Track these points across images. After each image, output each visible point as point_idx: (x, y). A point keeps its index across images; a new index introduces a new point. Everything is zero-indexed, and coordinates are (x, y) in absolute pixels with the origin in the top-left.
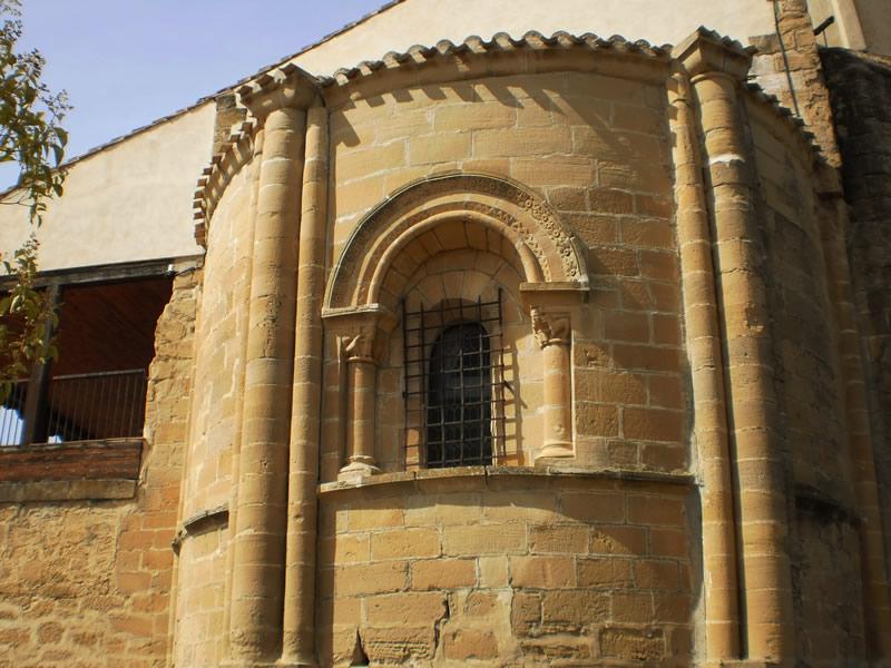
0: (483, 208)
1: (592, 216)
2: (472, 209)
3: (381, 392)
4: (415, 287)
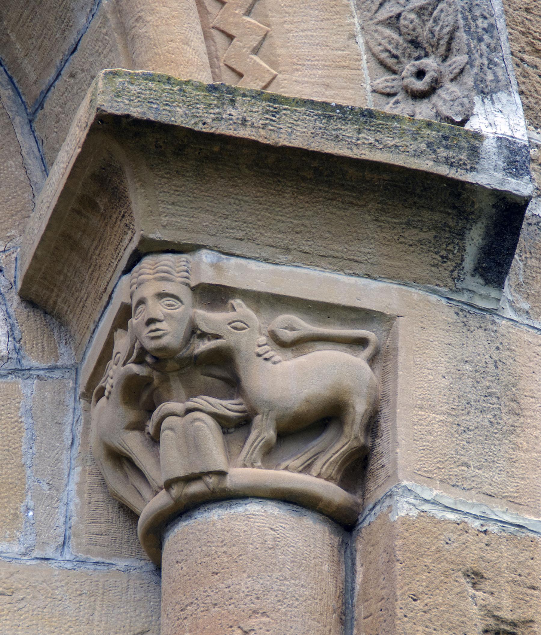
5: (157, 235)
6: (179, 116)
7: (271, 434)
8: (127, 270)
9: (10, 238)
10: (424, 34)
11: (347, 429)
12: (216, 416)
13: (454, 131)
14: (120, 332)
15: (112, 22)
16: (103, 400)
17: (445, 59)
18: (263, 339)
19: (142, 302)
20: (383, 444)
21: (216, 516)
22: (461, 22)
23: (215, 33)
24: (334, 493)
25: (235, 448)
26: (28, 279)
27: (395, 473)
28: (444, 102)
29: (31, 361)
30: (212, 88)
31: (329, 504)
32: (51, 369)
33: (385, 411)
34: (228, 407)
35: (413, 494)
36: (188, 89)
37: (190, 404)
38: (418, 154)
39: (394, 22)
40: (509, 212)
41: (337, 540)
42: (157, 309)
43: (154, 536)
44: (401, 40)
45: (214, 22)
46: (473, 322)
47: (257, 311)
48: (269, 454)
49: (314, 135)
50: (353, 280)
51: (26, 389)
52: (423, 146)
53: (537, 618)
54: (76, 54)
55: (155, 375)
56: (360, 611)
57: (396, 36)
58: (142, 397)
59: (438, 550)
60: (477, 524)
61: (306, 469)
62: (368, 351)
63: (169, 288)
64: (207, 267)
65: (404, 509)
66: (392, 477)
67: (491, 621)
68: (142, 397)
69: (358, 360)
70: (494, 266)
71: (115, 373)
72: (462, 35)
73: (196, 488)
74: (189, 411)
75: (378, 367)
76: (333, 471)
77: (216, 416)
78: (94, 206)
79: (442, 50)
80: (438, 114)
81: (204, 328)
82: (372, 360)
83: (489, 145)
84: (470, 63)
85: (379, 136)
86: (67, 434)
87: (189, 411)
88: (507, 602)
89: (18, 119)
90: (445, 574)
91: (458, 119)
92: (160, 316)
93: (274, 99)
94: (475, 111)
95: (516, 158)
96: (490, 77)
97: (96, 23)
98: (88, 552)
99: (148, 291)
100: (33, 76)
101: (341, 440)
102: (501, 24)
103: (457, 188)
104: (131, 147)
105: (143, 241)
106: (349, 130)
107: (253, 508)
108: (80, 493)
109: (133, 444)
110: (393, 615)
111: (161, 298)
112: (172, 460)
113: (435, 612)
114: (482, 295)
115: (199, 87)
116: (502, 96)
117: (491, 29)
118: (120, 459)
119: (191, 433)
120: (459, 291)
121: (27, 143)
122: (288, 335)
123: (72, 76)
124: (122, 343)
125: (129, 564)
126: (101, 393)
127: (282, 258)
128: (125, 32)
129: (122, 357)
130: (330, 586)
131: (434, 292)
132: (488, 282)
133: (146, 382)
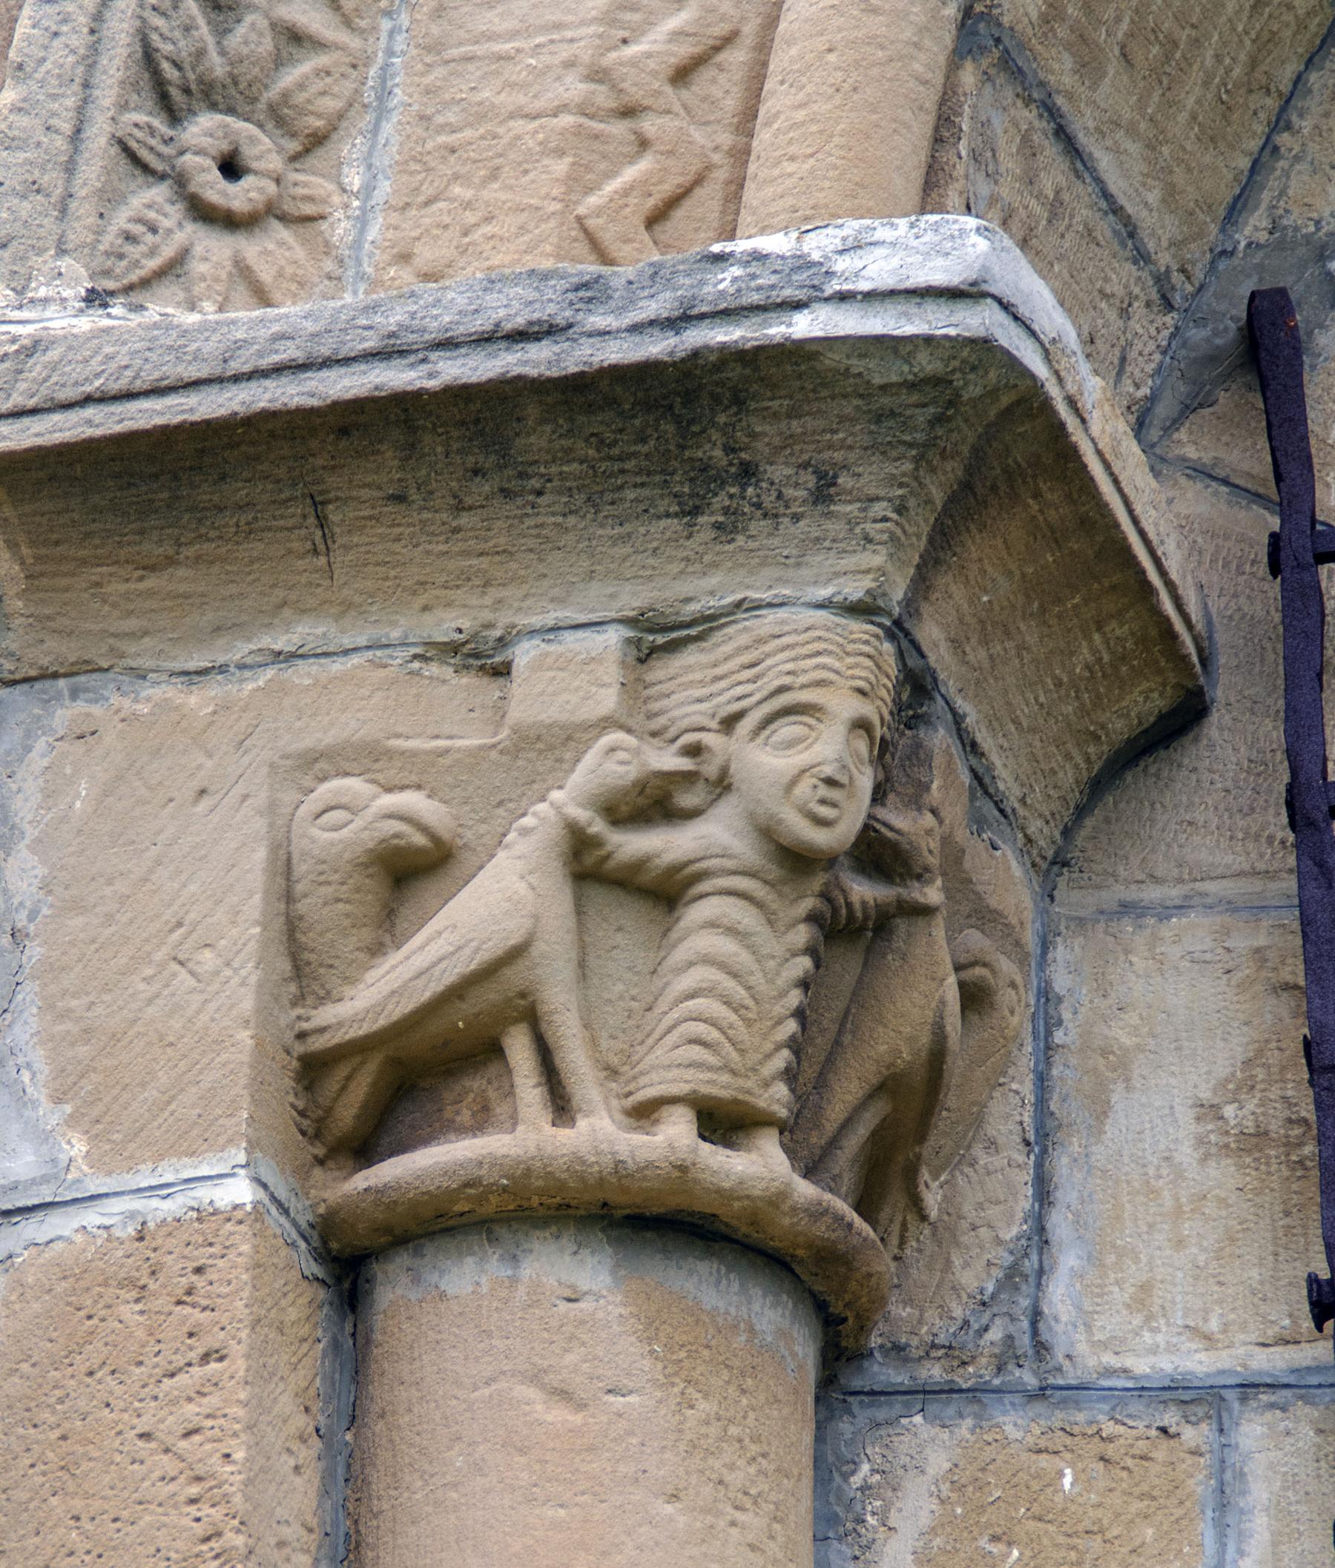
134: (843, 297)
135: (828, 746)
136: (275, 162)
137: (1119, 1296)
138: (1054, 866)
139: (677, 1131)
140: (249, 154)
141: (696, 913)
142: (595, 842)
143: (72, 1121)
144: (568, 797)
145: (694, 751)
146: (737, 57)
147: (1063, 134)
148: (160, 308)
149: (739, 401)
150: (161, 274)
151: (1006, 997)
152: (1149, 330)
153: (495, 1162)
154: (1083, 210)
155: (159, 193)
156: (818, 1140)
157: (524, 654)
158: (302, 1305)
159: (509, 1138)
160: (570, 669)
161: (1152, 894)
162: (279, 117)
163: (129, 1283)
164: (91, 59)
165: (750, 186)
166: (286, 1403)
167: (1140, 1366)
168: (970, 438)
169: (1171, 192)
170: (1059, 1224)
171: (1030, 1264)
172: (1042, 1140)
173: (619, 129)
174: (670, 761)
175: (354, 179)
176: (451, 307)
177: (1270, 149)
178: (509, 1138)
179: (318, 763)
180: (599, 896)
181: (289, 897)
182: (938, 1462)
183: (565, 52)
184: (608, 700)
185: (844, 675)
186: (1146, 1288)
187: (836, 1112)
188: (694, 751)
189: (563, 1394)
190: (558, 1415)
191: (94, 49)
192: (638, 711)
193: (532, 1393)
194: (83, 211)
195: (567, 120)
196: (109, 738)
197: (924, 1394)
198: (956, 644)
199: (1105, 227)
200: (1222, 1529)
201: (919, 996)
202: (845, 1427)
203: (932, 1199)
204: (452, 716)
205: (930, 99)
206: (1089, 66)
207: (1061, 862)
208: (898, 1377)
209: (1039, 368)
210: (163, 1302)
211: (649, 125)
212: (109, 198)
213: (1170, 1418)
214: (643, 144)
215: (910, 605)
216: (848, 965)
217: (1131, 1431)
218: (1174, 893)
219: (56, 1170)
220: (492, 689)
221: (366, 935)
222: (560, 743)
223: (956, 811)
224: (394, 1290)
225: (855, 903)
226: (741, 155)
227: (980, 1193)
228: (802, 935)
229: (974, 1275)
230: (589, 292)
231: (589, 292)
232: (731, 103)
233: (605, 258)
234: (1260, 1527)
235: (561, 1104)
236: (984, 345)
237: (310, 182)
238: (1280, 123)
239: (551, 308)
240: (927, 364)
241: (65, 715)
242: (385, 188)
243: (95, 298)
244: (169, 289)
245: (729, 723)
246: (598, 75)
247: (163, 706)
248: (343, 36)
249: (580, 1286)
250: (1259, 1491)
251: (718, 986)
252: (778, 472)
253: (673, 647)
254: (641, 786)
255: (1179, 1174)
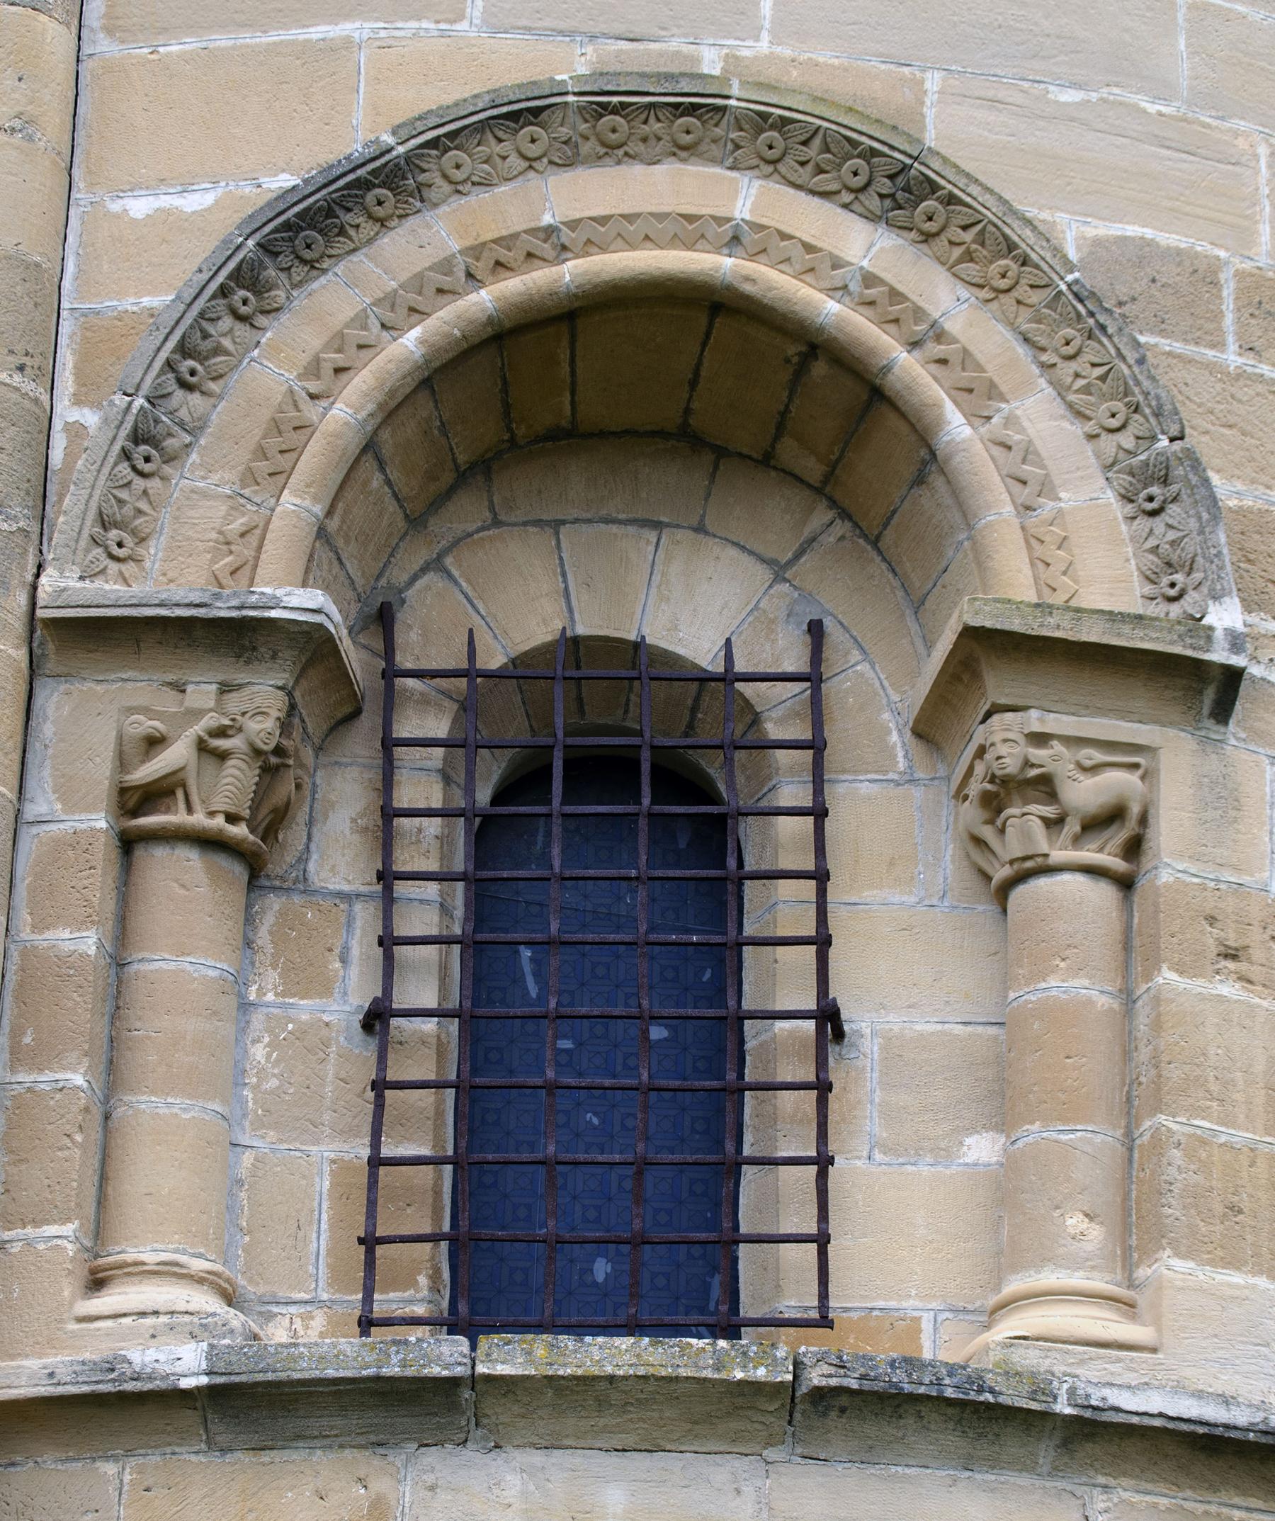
0: (813, 260)
1: (1240, 375)
2: (759, 253)
3: (266, 988)
4: (436, 565)
5: (1003, 701)
6: (1016, 625)
7: (1078, 828)
8: (983, 722)
9: (905, 692)
10: (1174, 558)
11: (1127, 824)
12: (1042, 818)
13: (1195, 625)
14: (977, 762)
15: (971, 556)
16: (967, 803)
17: (1189, 574)
18: (1072, 766)
19: (992, 745)
20: (1150, 833)
21: (1042, 882)
22: (1199, 551)
23: (1038, 562)
24: (1118, 864)
25: (1054, 838)
26: (917, 721)
27: (1159, 854)
28: (1189, 603)
29: (919, 775)
30: (1037, 605)
31: (1116, 872)
32: (932, 779)
33: (1152, 811)
34: (1050, 811)
35: (1170, 866)
36: (1021, 606)
37: (1025, 810)
38: (1172, 643)
39: (1155, 550)
40: (1232, 678)
41: (1121, 895)
42: (1003, 750)
43: (1003, 892)
44: (1159, 562)
45: (1037, 554)
46: (1209, 749)
47: (1067, 748)
48: (1077, 841)
49: (1104, 633)
50: (1130, 724)
51: (917, 793)
52: (1175, 637)
53: (1252, 944)
54: (950, 127)
55: (1002, 791)
56: (1137, 942)
57: (1156, 559)
58: (993, 804)
59: (1188, 903)
60: (1212, 884)
61: (1100, 850)
62: (1140, 772)
63: (1010, 735)
64: (1035, 720)
65: (1165, 877)
66: (1157, 855)
67: (1222, 948)
68: (993, 804)
69: (1133, 778)
70: (1222, 712)
71: (976, 787)
72: (1200, 560)
73: (1029, 864)
74: (1024, 814)
75: (1147, 781)
76: (1118, 851)
77: (1042, 818)
78: (960, 679)
79: (1187, 569)
80: (1185, 612)
81: (1034, 761)
82: (1143, 778)
83: (1219, 634)
84: (1205, 578)
85: (1146, 631)
86: (944, 823)
87: (1024, 814)
88: (1232, 936)
89: (908, 612)
90: (1192, 918)
91: (1198, 616)
92: (1004, 754)
93: (1078, 610)
94: (1209, 610)
95: (1236, 641)
96: (1219, 587)
97: (960, 556)
98: (959, 901)
99: (996, 738)
100: (917, 584)
101: (1123, 832)
102: (1225, 551)
103: (1199, 664)
104: (984, 647)
105: (993, 705)
106: (1126, 629)
107: (1066, 877)
108: (953, 862)
109: (987, 833)
110: (1159, 947)
111: (1006, 741)
112: (1013, 846)
113: (1186, 944)
114: (1215, 731)
115: (1029, 605)
116: (1226, 599)
117: (1219, 554)
118: (978, 841)
119: (1026, 827)
120: (1199, 729)
121: (914, 627)
122: (1088, 763)
123: (944, 587)
124: (980, 769)
125: (987, 908)
126: (966, 798)
127: (1084, 712)
128: (979, 564)
129: (980, 777)
130: (1118, 927)
131: (1183, 730)
132: (1218, 722)
133: (996, 795)
134: (285, 608)
135: (269, 724)
136: (131, 545)
137: (328, 868)
138: (319, 750)
139: (220, 821)
140: (125, 542)
141: (230, 763)
142: (205, 741)
143: (58, 799)
144: (199, 729)
145: (233, 720)
146: (258, 532)
147: (339, 559)
148: (99, 583)
149: (254, 630)
150: (99, 572)
151: (305, 786)
152: (355, 607)
153: (171, 823)
154: (342, 578)
155: (100, 550)
156: (255, 823)
157: (190, 688)
158: (115, 854)
159: (175, 817)
160: (202, 693)
161: (345, 760)
162: (133, 533)
163: (70, 845)
164: (85, 512)
165: (259, 569)
166: (110, 881)
167: (331, 887)
168: (311, 644)
169: (363, 572)
170: (313, 846)
171: (304, 857)
172: (310, 823)
173: (225, 547)
174: (227, 722)
175: (152, 551)
176: (179, 595)
177: (389, 561)
178: (175, 817)
179: (131, 710)
180: (204, 755)
181: (121, 745)
182: (276, 907)
183: (212, 525)
184: (212, 704)
185: (275, 704)
186: (334, 866)
187: (260, 817)
188: (233, 720)
189: (183, 886)
190: (182, 892)
191: (86, 510)
192: (219, 708)
193: (175, 885)
194: (80, 553)
195: (211, 544)
196: (75, 695)
197: (274, 889)
198: (303, 696)
199: (347, 582)
200: (348, 932)
201: (285, 788)
202: (252, 895)
203: (280, 837)
204: (168, 702)
205: (308, 551)
206: (347, 542)
207: (321, 748)
208: (268, 884)
209: (333, 631)
210: (79, 852)
211: (233, 548)
212: (88, 551)
213: (337, 901)
214: (231, 552)
215: (293, 688)
216: (267, 779)
217: (327, 904)
218: (349, 760)
219: (53, 812)
220: (180, 696)
221: (140, 758)
222: (198, 714)
223: (298, 740)
224: (139, 852)
225: (271, 764)
226: (257, 559)
227: (294, 836)
228: (257, 771)
229: (290, 858)
230: (217, 596)
231: (217, 596)
232: (255, 544)
233: (221, 586)
234: (358, 932)
235: (190, 810)
236: (321, 625)
237: (140, 551)
238: (392, 555)
239: (205, 600)
240: (305, 628)
241: (63, 687)
242: (160, 555)
243: (82, 578)
244: (102, 577)
245: (244, 714)
246: (220, 532)
247: (90, 688)
248: (152, 512)
249: (190, 859)
250: (359, 923)
251: (233, 783)
252: (263, 650)
253: (230, 691)
254: (219, 728)
255: (345, 836)
